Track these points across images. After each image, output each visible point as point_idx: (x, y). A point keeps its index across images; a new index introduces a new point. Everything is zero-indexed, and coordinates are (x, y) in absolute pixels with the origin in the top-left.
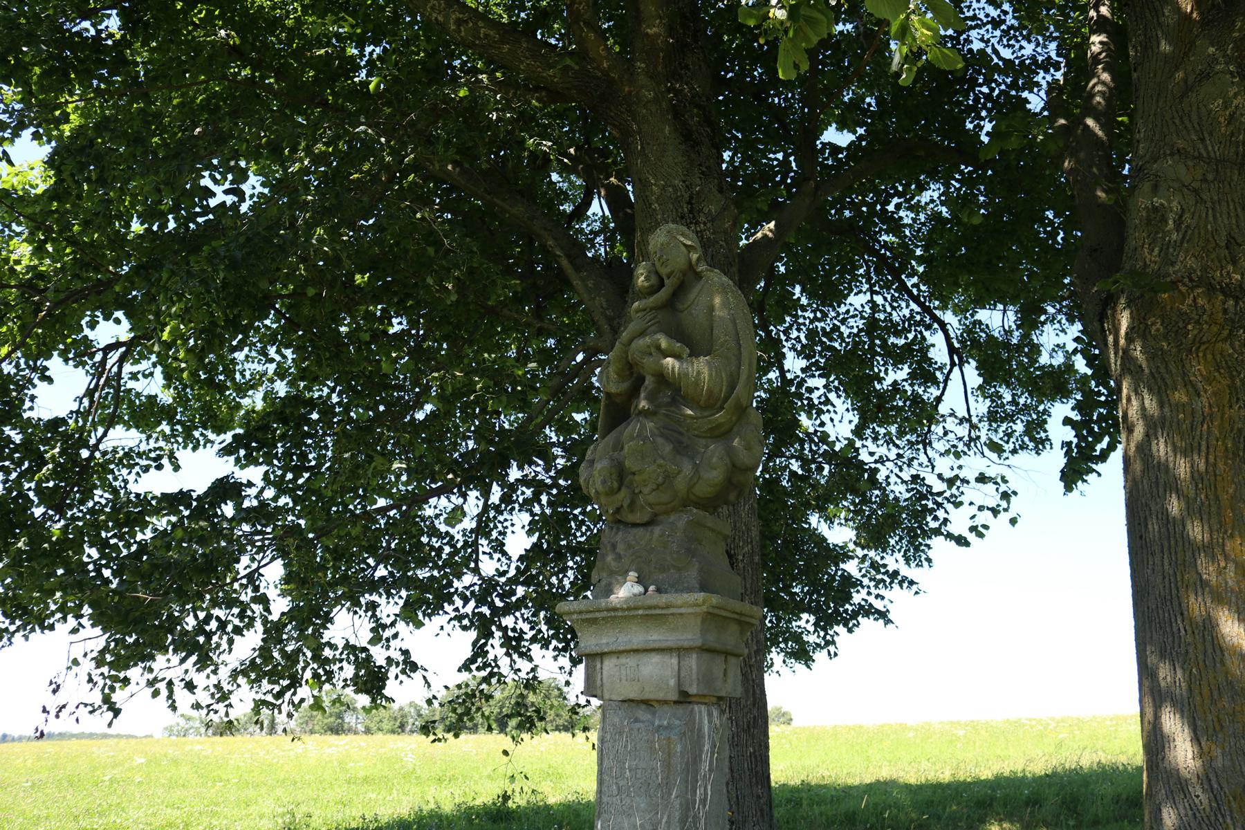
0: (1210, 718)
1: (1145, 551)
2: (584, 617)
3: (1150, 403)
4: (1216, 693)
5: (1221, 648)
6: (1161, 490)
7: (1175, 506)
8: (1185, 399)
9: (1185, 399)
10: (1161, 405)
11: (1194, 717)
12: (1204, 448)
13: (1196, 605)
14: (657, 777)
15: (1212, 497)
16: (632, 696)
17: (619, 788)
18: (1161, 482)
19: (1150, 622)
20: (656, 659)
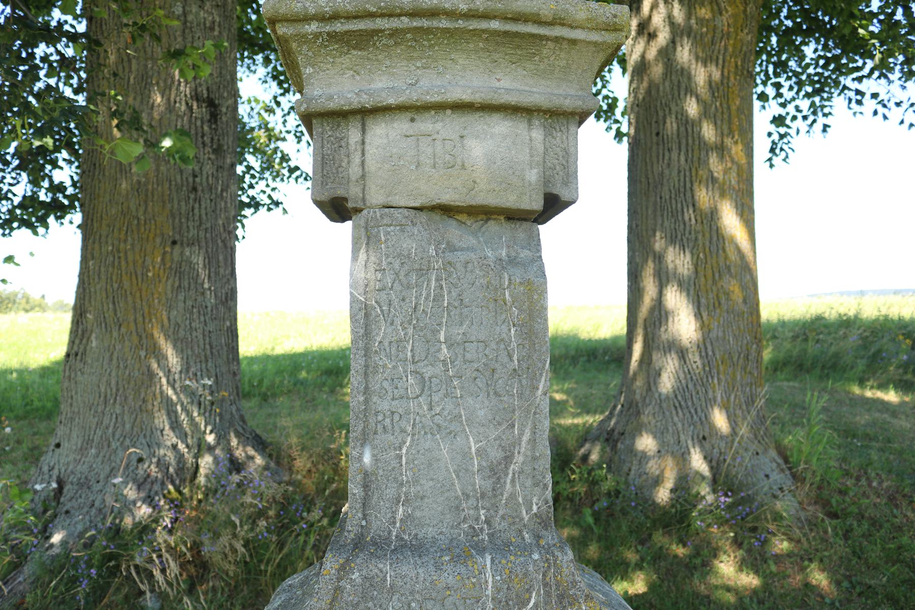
0: (711, 296)
1: (661, 147)
2: (339, 27)
3: (678, 12)
4: (717, 275)
5: (723, 237)
6: (682, 93)
7: (692, 108)
8: (708, 16)
9: (708, 16)
10: (689, 16)
11: (698, 296)
12: (721, 61)
13: (703, 196)
14: (510, 357)
15: (725, 106)
16: (447, 197)
17: (422, 381)
18: (683, 85)
19: (662, 210)
20: (501, 126)
